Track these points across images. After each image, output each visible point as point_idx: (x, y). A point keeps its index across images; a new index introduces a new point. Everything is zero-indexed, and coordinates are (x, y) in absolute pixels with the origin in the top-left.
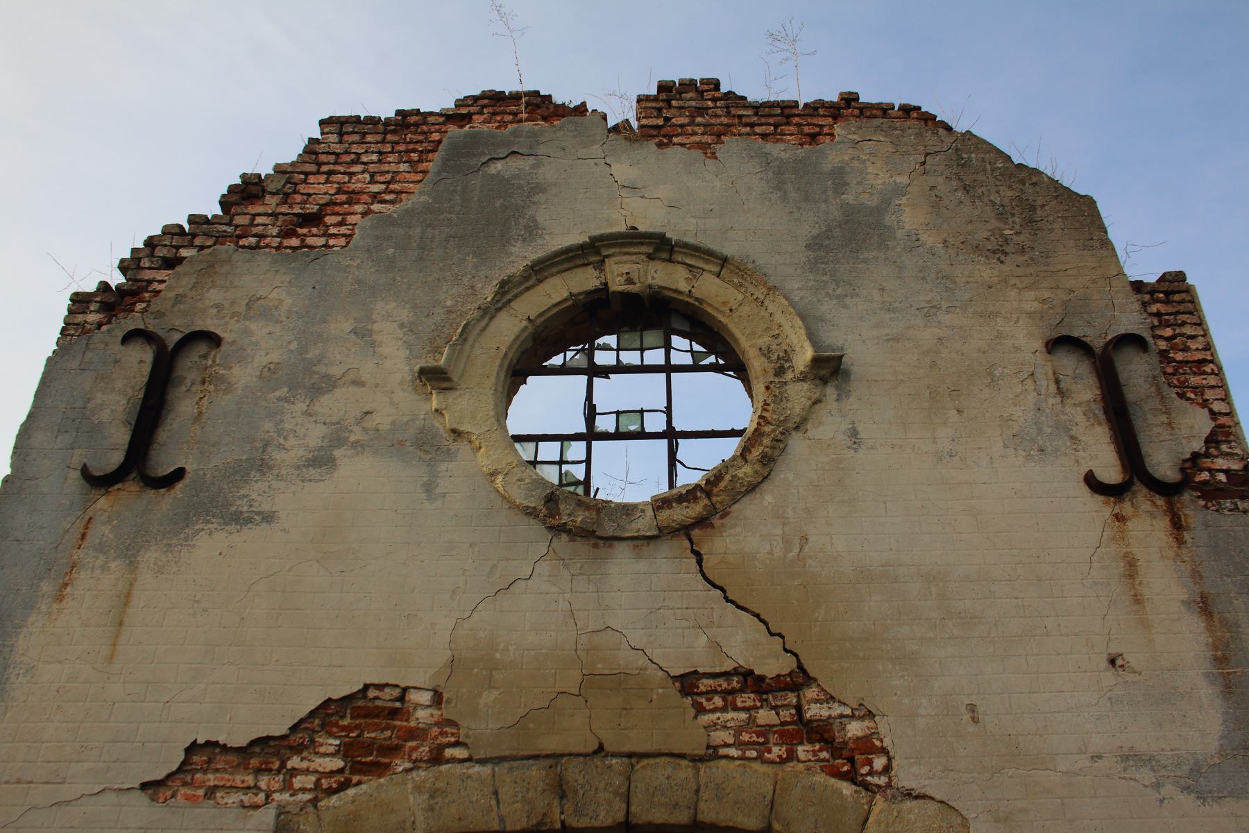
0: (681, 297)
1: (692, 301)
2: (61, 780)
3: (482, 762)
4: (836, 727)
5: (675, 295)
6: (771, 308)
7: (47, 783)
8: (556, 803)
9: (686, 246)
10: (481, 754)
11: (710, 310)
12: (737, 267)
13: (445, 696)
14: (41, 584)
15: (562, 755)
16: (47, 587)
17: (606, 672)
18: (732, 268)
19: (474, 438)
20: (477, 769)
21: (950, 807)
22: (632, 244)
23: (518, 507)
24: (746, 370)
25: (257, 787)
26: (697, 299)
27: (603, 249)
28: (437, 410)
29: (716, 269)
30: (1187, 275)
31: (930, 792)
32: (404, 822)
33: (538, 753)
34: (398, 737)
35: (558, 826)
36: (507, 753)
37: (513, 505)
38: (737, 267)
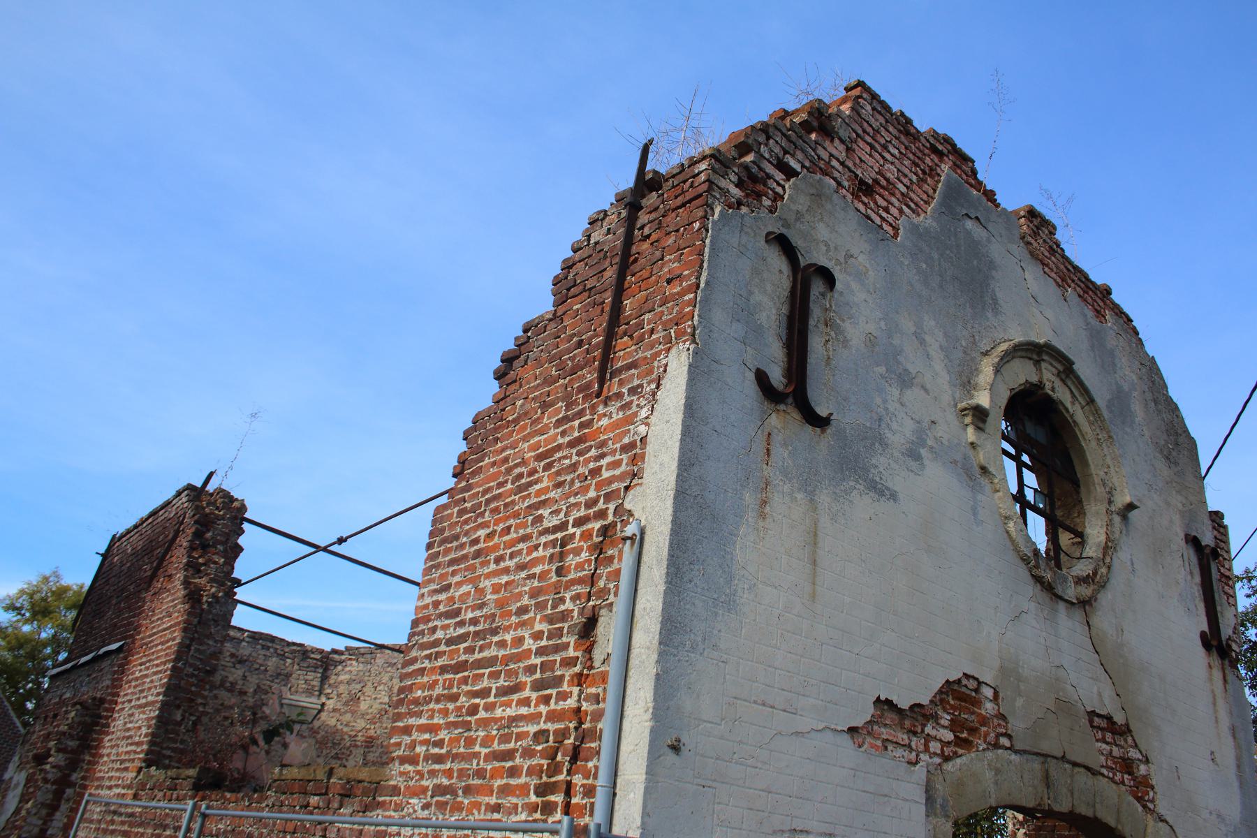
0: (1067, 415)
1: (1071, 421)
2: (794, 711)
3: (1016, 752)
4: (1135, 766)
5: (1064, 411)
6: (1106, 451)
7: (785, 711)
8: (1045, 790)
9: (1078, 378)
10: (1018, 746)
11: (1078, 433)
12: (1096, 410)
13: (1001, 695)
14: (744, 492)
15: (1049, 756)
16: (749, 498)
17: (1064, 699)
18: (1093, 409)
19: (996, 481)
20: (1013, 757)
21: (1173, 830)
22: (1056, 359)
23: (1019, 552)
24: (1076, 484)
25: (909, 746)
26: (1074, 422)
27: (1043, 354)
28: (972, 443)
29: (1083, 403)
30: (1225, 517)
31: (1168, 819)
32: (985, 791)
33: (1039, 751)
34: (978, 722)
35: (1047, 808)
36: (1027, 748)
37: (1017, 550)
38: (1096, 410)
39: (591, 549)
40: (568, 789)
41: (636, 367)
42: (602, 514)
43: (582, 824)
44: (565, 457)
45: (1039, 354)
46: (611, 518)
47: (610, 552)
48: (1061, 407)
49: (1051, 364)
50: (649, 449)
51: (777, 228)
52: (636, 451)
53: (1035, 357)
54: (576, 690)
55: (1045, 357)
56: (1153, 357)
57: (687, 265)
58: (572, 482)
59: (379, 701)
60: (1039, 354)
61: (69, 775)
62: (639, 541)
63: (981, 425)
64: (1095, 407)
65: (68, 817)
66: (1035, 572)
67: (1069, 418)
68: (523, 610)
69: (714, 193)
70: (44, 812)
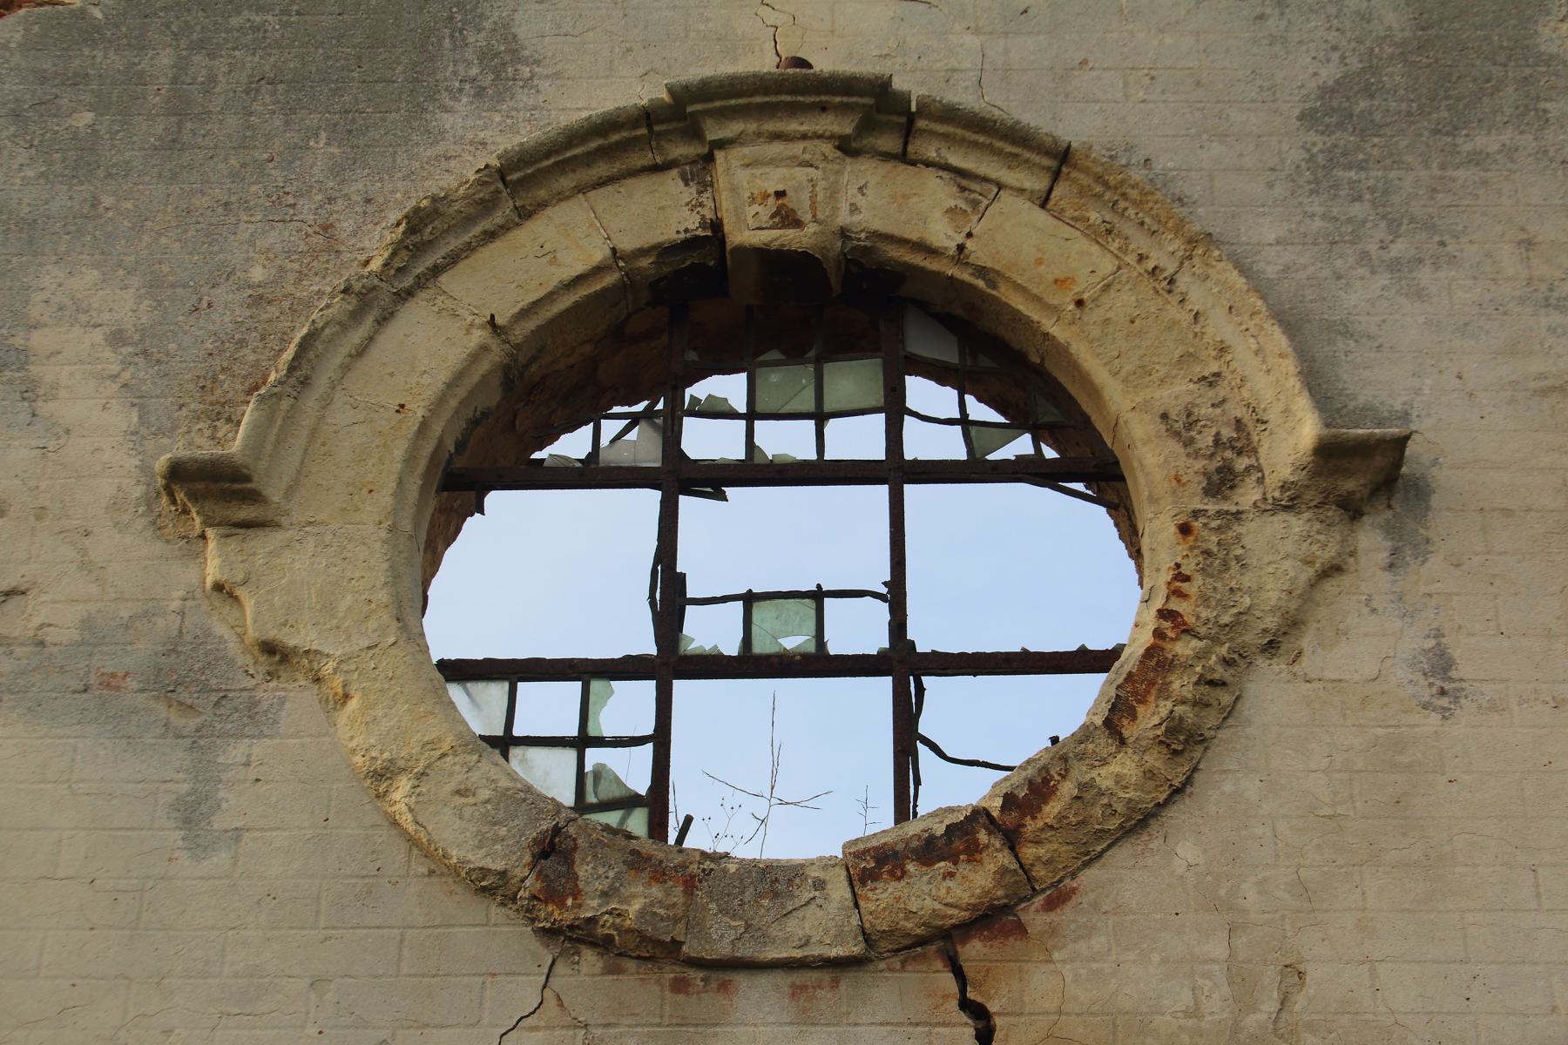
0: (933, 265)
5: (917, 260)
6: (1197, 298)
12: (1099, 179)
18: (1085, 180)
19: (328, 668)
22: (794, 110)
23: (454, 871)
26: (981, 271)
28: (219, 587)
38: (1099, 179)
45: (693, 132)
48: (895, 253)
49: (778, 136)
51: (813, 940)
53: (681, 150)
55: (714, 132)
56: (671, 90)
60: (693, 132)
63: (246, 512)
64: (1086, 171)
66: (552, 914)
67: (952, 271)
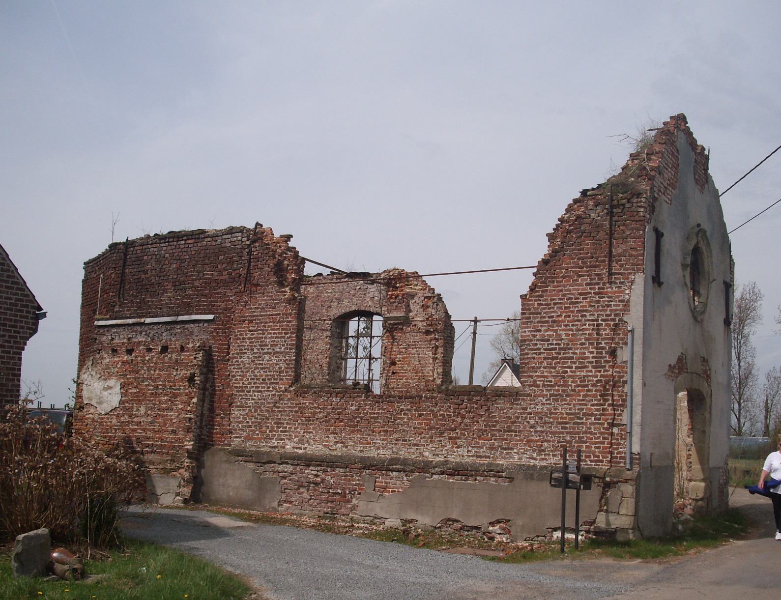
39: (612, 330)
40: (613, 395)
41: (621, 275)
42: (614, 320)
43: (16, 565)
44: (593, 297)
46: (617, 322)
47: (619, 332)
50: (631, 304)
52: (626, 304)
54: (611, 370)
57: (639, 246)
58: (598, 307)
59: (197, 359)
61: (206, 385)
62: (632, 331)
65: (210, 405)
68: (582, 344)
69: (696, 298)
70: (201, 403)
